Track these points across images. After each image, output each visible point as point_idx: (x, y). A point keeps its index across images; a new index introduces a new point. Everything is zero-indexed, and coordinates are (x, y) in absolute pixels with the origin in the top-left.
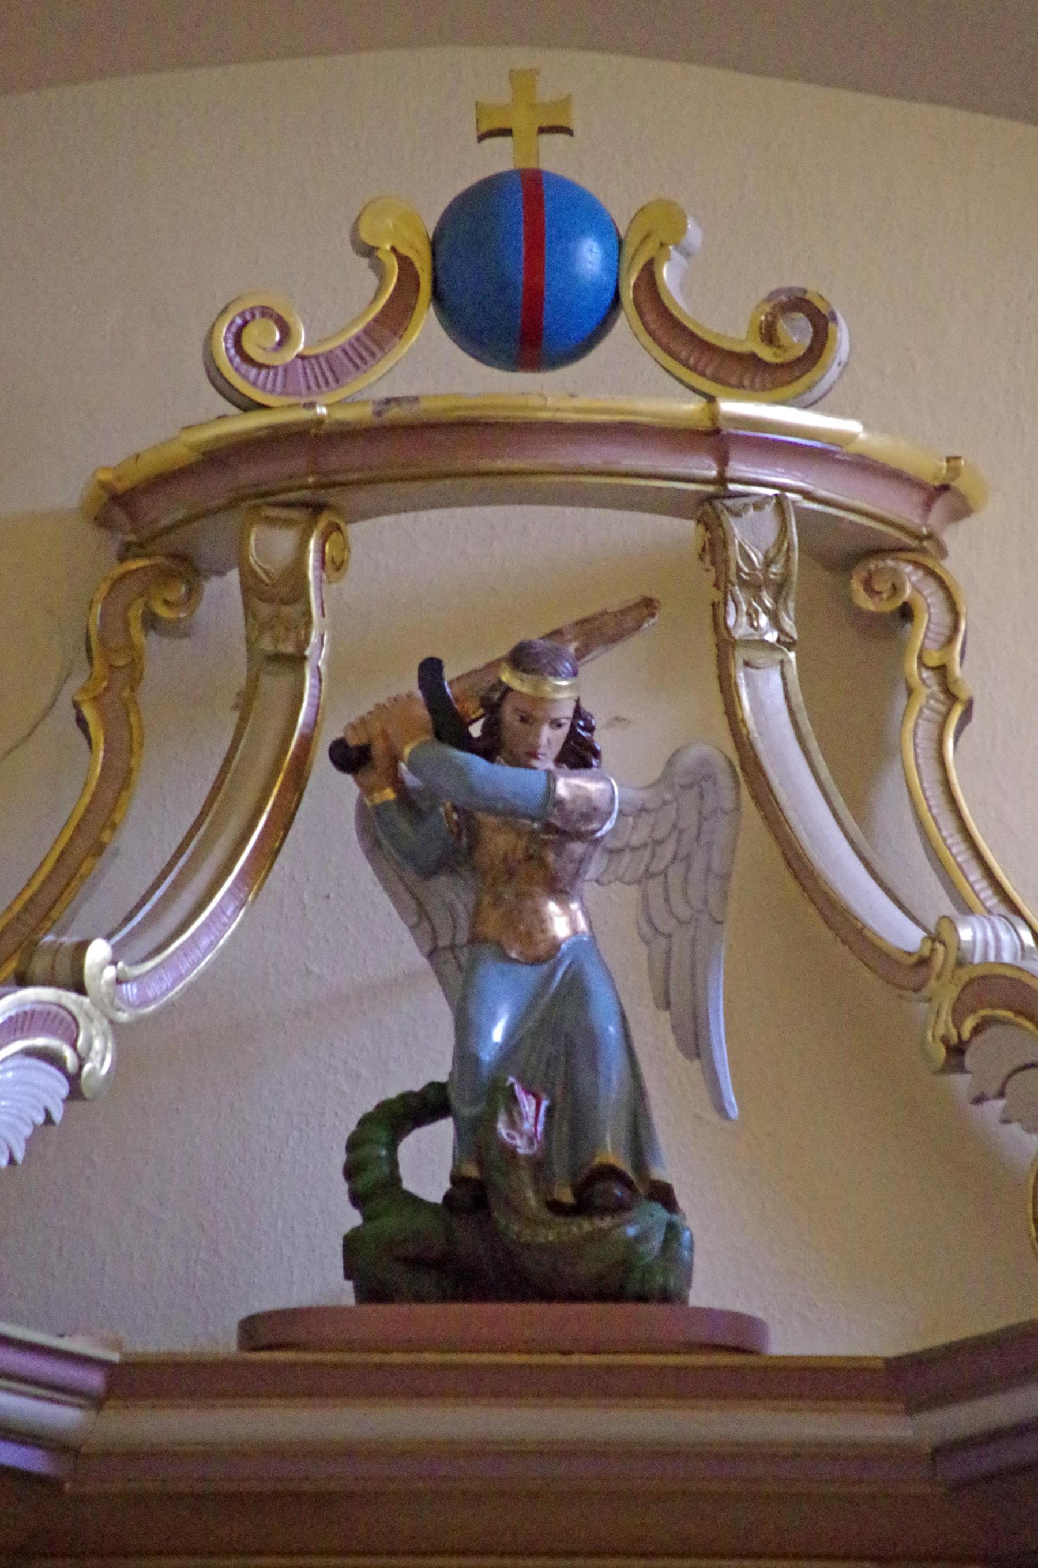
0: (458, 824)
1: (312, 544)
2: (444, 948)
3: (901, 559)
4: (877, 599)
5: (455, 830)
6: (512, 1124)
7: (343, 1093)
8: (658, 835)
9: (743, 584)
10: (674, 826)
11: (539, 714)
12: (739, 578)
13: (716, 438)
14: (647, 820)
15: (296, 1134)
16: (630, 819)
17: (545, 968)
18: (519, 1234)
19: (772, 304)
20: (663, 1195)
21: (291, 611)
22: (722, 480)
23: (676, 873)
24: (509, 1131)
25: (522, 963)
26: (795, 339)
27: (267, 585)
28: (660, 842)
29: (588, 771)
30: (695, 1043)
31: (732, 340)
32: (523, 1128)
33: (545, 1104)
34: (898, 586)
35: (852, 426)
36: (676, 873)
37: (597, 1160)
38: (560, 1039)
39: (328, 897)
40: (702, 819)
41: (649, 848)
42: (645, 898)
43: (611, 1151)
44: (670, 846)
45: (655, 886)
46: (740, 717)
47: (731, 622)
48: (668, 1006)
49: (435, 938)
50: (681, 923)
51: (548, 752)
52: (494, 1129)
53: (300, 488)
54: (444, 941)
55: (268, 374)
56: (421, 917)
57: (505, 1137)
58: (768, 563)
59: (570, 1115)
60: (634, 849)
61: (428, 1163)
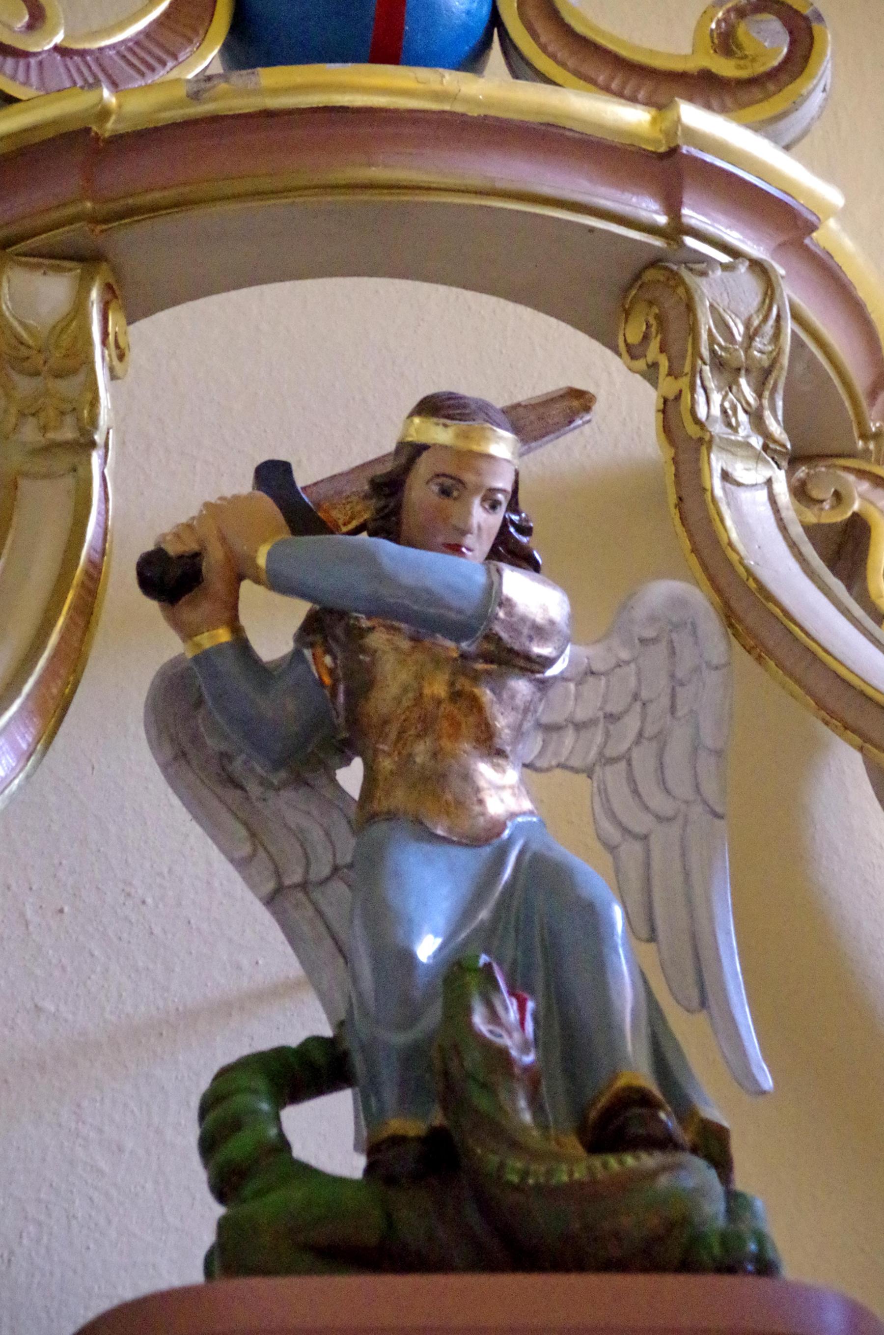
0: (331, 672)
1: (94, 294)
2: (296, 886)
3: (835, 466)
4: (816, 508)
5: (327, 680)
6: (494, 1017)
7: (100, 1172)
8: (613, 707)
9: (719, 364)
10: (636, 697)
11: (469, 477)
12: (713, 352)
13: (669, 168)
14: (594, 689)
15: (32, 1228)
16: (572, 686)
17: (486, 851)
18: (525, 1174)
19: (724, 9)
20: (714, 1146)
21: (66, 387)
22: (677, 230)
23: (644, 760)
24: (491, 1027)
25: (453, 842)
26: (766, 44)
27: (29, 347)
28: (612, 718)
29: (536, 575)
30: (705, 996)
31: (670, 56)
32: (509, 1025)
33: (530, 1005)
34: (843, 492)
35: (832, 195)
36: (644, 760)
37: (621, 1083)
38: (534, 924)
39: (61, 911)
40: (676, 683)
41: (601, 725)
42: (603, 791)
43: (639, 1071)
44: (632, 723)
45: (614, 776)
46: (725, 541)
47: (702, 412)
48: (652, 937)
49: (278, 874)
50: (660, 819)
51: (477, 546)
52: (470, 1025)
53: (72, 220)
54: (295, 877)
55: (28, 66)
56: (254, 849)
57: (488, 1035)
58: (750, 337)
59: (572, 1033)
60: (579, 727)
61: (326, 1134)
